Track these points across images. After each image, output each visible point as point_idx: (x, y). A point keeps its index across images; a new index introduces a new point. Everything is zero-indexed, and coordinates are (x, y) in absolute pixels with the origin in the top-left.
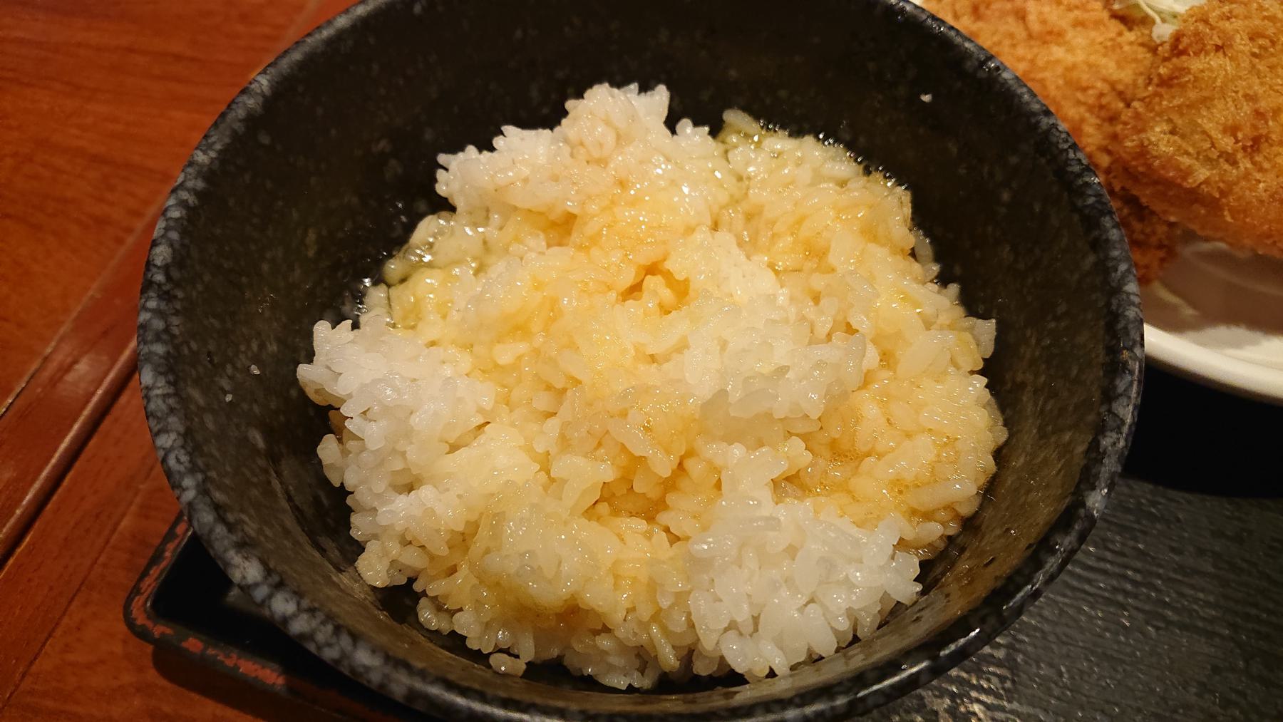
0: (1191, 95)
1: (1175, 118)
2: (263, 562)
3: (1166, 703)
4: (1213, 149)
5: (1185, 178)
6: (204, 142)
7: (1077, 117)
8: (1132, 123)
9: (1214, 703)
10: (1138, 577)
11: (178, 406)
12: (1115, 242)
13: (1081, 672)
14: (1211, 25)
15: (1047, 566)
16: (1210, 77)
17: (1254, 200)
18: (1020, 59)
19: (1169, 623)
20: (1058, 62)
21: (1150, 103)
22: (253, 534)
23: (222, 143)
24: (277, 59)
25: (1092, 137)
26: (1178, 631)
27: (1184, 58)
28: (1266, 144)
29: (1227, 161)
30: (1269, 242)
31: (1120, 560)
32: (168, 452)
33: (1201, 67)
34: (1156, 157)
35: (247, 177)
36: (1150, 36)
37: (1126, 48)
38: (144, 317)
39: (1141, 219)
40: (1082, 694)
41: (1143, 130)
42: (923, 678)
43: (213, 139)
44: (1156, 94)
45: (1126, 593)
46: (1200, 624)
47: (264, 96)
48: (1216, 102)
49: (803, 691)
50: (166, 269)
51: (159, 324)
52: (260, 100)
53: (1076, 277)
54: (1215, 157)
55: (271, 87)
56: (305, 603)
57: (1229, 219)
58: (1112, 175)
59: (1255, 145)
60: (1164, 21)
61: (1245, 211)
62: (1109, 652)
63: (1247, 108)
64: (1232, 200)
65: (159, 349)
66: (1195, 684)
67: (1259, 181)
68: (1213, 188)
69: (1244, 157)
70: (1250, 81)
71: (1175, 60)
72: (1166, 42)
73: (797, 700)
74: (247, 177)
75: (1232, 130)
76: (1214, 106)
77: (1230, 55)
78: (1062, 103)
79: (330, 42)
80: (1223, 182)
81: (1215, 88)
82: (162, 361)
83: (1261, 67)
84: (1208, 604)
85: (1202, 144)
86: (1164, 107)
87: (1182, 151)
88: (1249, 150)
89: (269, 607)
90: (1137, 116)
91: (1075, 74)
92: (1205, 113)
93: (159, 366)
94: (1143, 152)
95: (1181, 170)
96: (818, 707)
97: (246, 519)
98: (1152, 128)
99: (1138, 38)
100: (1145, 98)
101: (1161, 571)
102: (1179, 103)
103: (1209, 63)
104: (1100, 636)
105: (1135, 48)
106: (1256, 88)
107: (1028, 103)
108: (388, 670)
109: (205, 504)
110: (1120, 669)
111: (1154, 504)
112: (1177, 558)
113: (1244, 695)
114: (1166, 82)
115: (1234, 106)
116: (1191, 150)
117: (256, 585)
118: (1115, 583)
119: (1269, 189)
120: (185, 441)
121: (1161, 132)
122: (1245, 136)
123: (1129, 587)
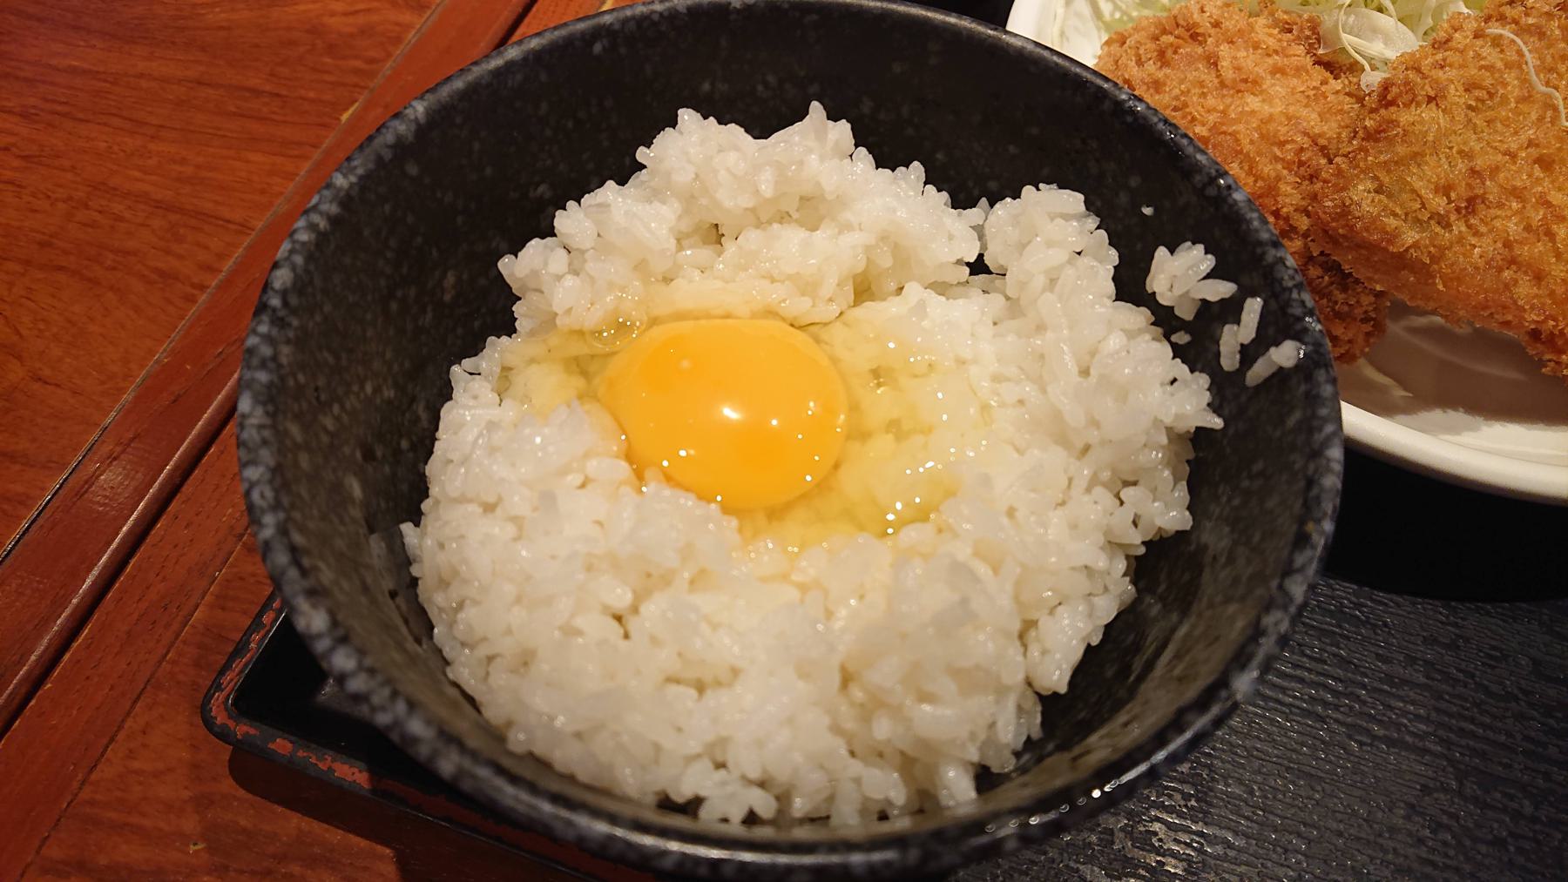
2: (332, 614)
5: (1390, 242)
6: (346, 164)
7: (1273, 174)
9: (1423, 826)
16: (1420, 131)
19: (1375, 737)
20: (1253, 112)
21: (1354, 158)
24: (437, 85)
25: (1290, 196)
27: (1393, 109)
28: (1482, 205)
29: (1439, 223)
31: (1319, 667)
32: (252, 485)
35: (387, 208)
38: (252, 341)
39: (1344, 289)
43: (355, 163)
44: (1361, 149)
45: (1326, 704)
46: (1409, 739)
50: (284, 294)
51: (266, 351)
52: (413, 127)
53: (1278, 433)
56: (368, 662)
57: (1441, 287)
59: (1471, 206)
60: (1374, 68)
61: (1458, 279)
63: (1462, 166)
64: (1444, 267)
65: (263, 377)
66: (1402, 805)
67: (1475, 246)
71: (1383, 111)
74: (387, 208)
75: (1445, 190)
77: (1443, 107)
79: (498, 73)
80: (1434, 246)
83: (1479, 121)
84: (1418, 717)
85: (1411, 204)
86: (1370, 163)
88: (1464, 212)
90: (1339, 173)
91: (1272, 127)
94: (1344, 212)
95: (1387, 233)
97: (322, 565)
99: (1344, 88)
100: (1349, 153)
103: (1420, 115)
105: (1341, 97)
106: (1472, 144)
107: (1257, 231)
111: (1358, 606)
113: (1456, 817)
114: (1372, 136)
115: (1447, 163)
116: (1398, 210)
117: (320, 636)
122: (1459, 198)
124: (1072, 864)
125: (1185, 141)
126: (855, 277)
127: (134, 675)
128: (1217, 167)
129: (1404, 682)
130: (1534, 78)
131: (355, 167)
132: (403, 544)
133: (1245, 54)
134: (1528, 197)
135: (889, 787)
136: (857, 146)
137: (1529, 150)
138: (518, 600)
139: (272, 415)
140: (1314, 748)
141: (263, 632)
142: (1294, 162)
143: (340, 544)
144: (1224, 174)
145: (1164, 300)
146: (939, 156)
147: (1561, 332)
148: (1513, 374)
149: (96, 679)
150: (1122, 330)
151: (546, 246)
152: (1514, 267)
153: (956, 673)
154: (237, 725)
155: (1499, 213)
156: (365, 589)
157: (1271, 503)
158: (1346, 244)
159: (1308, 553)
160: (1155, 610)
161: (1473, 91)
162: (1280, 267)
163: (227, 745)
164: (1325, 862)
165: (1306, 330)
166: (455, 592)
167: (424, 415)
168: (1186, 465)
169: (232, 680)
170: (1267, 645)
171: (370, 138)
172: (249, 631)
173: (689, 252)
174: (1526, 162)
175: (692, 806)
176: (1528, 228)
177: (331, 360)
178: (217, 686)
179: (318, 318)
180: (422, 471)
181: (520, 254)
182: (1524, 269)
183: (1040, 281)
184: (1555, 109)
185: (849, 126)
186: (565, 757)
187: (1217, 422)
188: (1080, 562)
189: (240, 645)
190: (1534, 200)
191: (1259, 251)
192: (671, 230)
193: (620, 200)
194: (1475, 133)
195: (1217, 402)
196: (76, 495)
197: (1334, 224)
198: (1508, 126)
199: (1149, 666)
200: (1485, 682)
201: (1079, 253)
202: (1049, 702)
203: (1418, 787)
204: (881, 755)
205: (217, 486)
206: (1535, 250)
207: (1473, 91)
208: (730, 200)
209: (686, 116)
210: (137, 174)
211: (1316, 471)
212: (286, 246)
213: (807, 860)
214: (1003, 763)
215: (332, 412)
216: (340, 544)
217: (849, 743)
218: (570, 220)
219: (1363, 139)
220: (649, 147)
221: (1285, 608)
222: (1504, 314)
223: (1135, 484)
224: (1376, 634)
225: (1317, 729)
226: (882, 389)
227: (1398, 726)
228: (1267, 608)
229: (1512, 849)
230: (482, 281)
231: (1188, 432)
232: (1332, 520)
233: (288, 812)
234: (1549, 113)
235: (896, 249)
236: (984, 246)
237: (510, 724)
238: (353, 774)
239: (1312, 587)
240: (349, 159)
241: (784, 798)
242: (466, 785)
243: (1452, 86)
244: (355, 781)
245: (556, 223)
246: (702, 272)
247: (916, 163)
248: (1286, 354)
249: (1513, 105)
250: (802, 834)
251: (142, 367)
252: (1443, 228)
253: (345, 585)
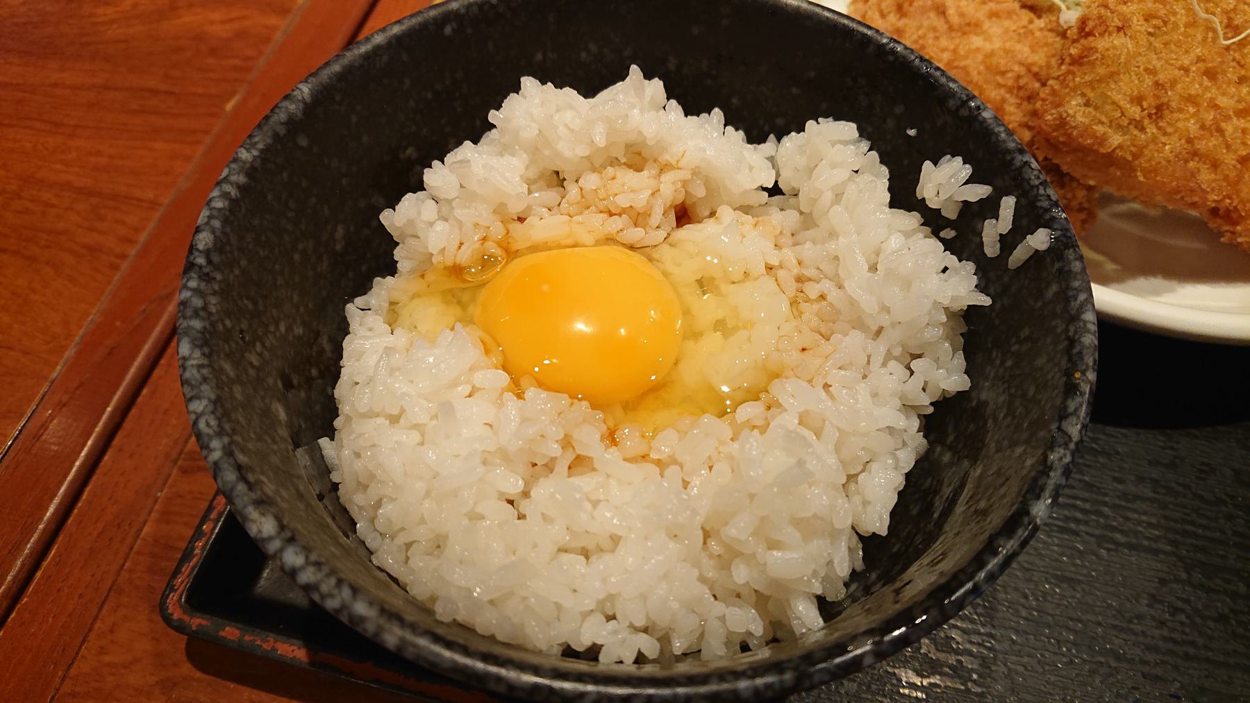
0: (1099, 71)
1: (1088, 91)
2: (278, 519)
3: (1123, 616)
4: (1123, 118)
6: (248, 141)
7: (998, 98)
8: (1050, 99)
10: (1087, 506)
11: (210, 376)
13: (1045, 594)
14: (1111, 10)
15: (989, 567)
16: (1115, 55)
17: (1162, 161)
18: (943, 50)
19: (1118, 544)
20: (978, 50)
21: (1064, 80)
22: (270, 493)
23: (264, 143)
24: (318, 70)
25: (1014, 114)
26: (1126, 551)
27: (1091, 39)
29: (1136, 127)
30: (1178, 197)
33: (1107, 46)
34: (1075, 127)
35: (285, 175)
36: (1058, 21)
37: (1038, 34)
40: (1048, 614)
41: (1059, 105)
42: (868, 661)
43: (256, 139)
44: (1069, 72)
46: (1146, 543)
47: (303, 101)
48: (1122, 76)
49: (755, 665)
50: (207, 253)
51: (197, 302)
52: (301, 106)
53: (1039, 304)
54: (1126, 125)
55: (312, 95)
56: (313, 557)
57: (1141, 179)
58: (1035, 147)
59: (1159, 111)
60: (1068, 8)
62: (1068, 574)
63: (1149, 81)
64: (1143, 162)
65: (197, 324)
67: (1165, 144)
68: (1126, 152)
69: (1151, 123)
70: (1149, 57)
71: (1083, 41)
72: (1072, 27)
73: (749, 673)
74: (285, 175)
75: (1138, 100)
76: (1121, 80)
78: (985, 86)
80: (1135, 146)
81: (1120, 64)
82: (200, 335)
83: (1158, 44)
84: (1150, 525)
85: (1113, 114)
87: (1097, 121)
89: (281, 559)
90: (1054, 93)
91: (994, 60)
92: (1113, 87)
93: (196, 339)
94: (1062, 123)
96: (769, 679)
97: (264, 478)
98: (1069, 102)
99: (1046, 24)
100: (1059, 76)
101: (1107, 499)
102: (1090, 78)
104: (1057, 560)
105: (1046, 33)
106: (1154, 63)
107: (1004, 141)
108: (382, 621)
109: (229, 463)
110: (1079, 589)
111: (1095, 440)
112: (1120, 487)
114: (1077, 61)
116: (1104, 119)
117: (270, 538)
118: (1066, 512)
119: (1174, 150)
120: (215, 408)
121: (1077, 105)
123: (1079, 515)
124: (890, 669)
125: (938, 73)
126: (676, 207)
127: (98, 583)
128: (966, 92)
129: (1138, 498)
130: (1197, 7)
131: (256, 143)
132: (323, 456)
133: (966, 3)
134: (1201, 102)
135: (749, 622)
136: (668, 99)
137: (1198, 65)
138: (428, 494)
139: (208, 356)
140: (1071, 557)
142: (1014, 87)
143: (275, 460)
144: (973, 98)
145: (933, 204)
146: (734, 101)
147: (1235, 208)
148: (1195, 245)
149: (66, 590)
150: (899, 231)
151: (418, 199)
152: (1197, 159)
153: (798, 523)
154: (192, 618)
155: (1181, 116)
156: (300, 496)
157: (1040, 361)
158: (1065, 149)
159: (1078, 400)
160: (947, 458)
161: (1151, 20)
162: (1026, 169)
163: (181, 636)
164: (1090, 647)
165: (1053, 219)
166: (374, 493)
167: (327, 347)
168: (960, 337)
169: (183, 582)
170: (1055, 477)
171: (267, 118)
173: (537, 195)
174: (1197, 74)
175: (593, 653)
176: (1203, 127)
177: (250, 306)
178: (170, 587)
180: (330, 393)
181: (397, 207)
182: (1203, 159)
183: (828, 196)
184: (1214, 31)
185: (661, 83)
186: (486, 622)
187: (986, 301)
188: (883, 425)
189: (187, 552)
190: (1205, 104)
191: (1009, 158)
192: (521, 177)
193: (476, 155)
194: (1156, 54)
195: (983, 283)
196: (34, 438)
197: (1055, 134)
198: (1180, 47)
199: (952, 502)
200: (1200, 492)
201: (857, 172)
202: (870, 543)
203: (1156, 580)
204: (738, 596)
206: (1209, 144)
207: (1151, 20)
208: (569, 151)
209: (528, 83)
210: (59, 167)
211: (1076, 332)
212: (205, 213)
213: (703, 689)
214: (837, 593)
215: (255, 349)
216: (275, 460)
217: (711, 589)
218: (435, 176)
219: (1070, 64)
220: (497, 110)
221: (1066, 445)
222: (1191, 197)
223: (920, 356)
224: (1111, 461)
225: (1073, 541)
226: (707, 296)
227: (1136, 533)
228: (1051, 447)
229: (1233, 622)
230: (366, 232)
231: (962, 309)
232: (1094, 370)
233: (239, 687)
234: (1210, 35)
235: (707, 182)
236: (778, 175)
237: (433, 599)
238: (293, 651)
239: (1084, 427)
240: (250, 136)
241: (665, 640)
242: (409, 653)
243: (1135, 17)
244: (295, 657)
245: (425, 178)
246: (550, 210)
247: (716, 110)
248: (1040, 239)
249: (1182, 29)
250: (683, 668)
251: (80, 327)
252: (1140, 131)
253: (284, 494)
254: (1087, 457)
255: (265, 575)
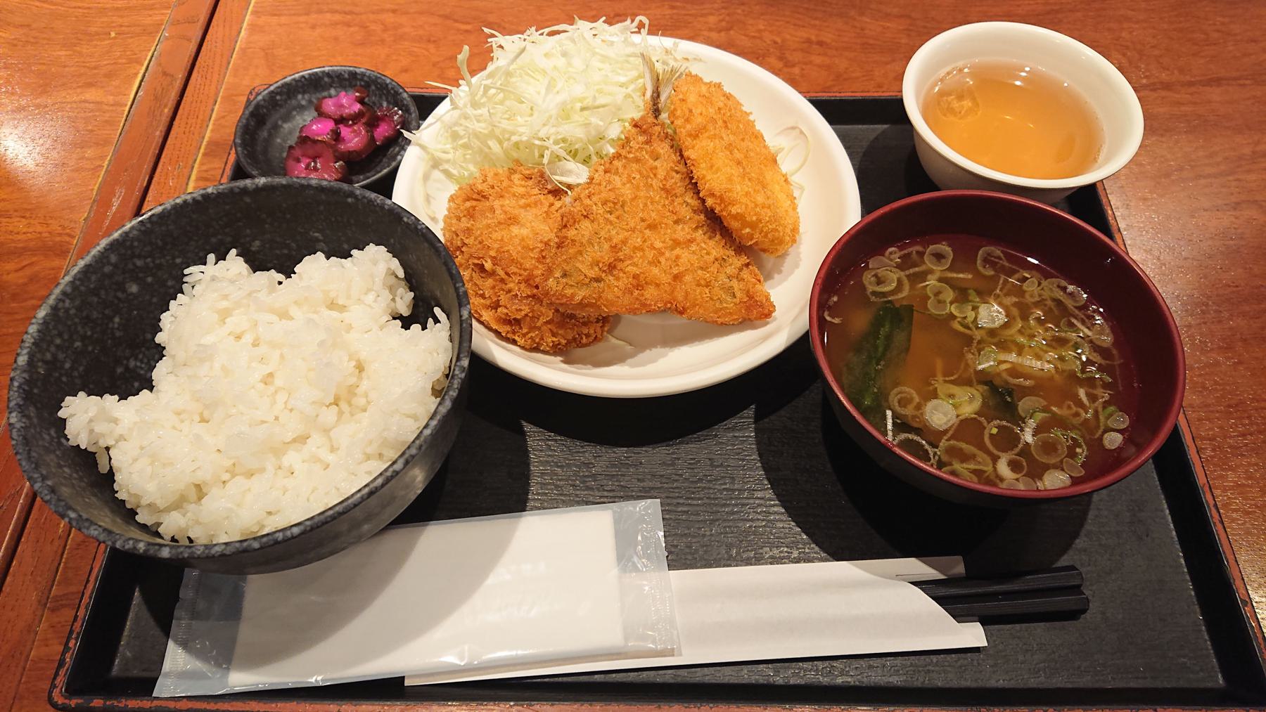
12: (260, 543)
63: (606, 246)
83: (612, 218)
141: (71, 651)
166: (707, 235)
172: (63, 654)
178: (53, 686)
179: (163, 228)
205: (23, 582)
254: (623, 470)
255: (116, 663)
